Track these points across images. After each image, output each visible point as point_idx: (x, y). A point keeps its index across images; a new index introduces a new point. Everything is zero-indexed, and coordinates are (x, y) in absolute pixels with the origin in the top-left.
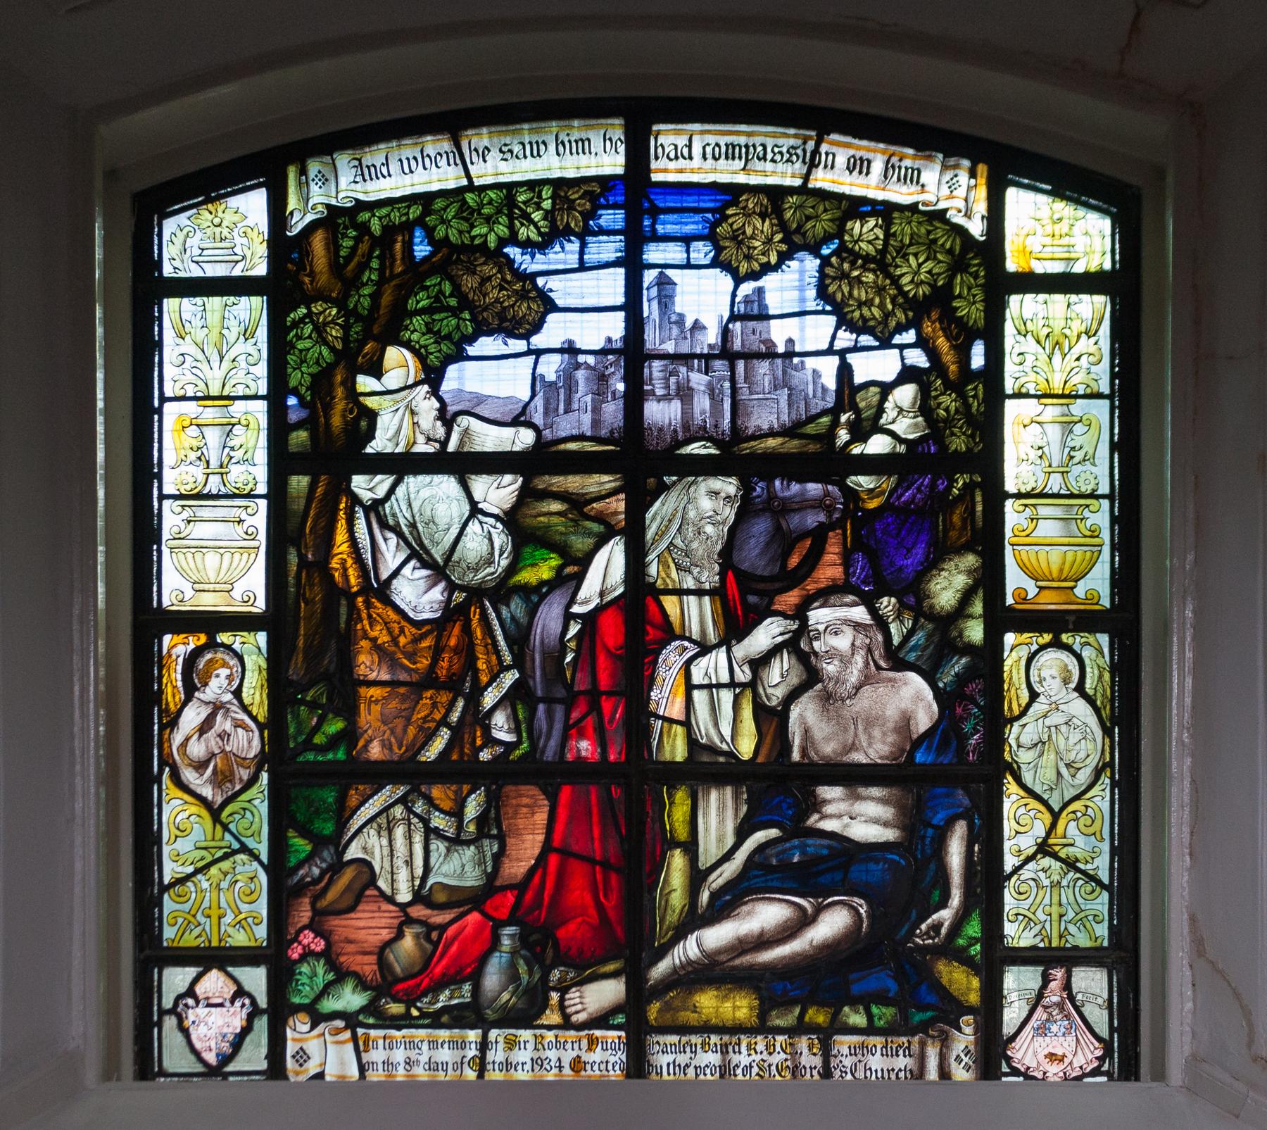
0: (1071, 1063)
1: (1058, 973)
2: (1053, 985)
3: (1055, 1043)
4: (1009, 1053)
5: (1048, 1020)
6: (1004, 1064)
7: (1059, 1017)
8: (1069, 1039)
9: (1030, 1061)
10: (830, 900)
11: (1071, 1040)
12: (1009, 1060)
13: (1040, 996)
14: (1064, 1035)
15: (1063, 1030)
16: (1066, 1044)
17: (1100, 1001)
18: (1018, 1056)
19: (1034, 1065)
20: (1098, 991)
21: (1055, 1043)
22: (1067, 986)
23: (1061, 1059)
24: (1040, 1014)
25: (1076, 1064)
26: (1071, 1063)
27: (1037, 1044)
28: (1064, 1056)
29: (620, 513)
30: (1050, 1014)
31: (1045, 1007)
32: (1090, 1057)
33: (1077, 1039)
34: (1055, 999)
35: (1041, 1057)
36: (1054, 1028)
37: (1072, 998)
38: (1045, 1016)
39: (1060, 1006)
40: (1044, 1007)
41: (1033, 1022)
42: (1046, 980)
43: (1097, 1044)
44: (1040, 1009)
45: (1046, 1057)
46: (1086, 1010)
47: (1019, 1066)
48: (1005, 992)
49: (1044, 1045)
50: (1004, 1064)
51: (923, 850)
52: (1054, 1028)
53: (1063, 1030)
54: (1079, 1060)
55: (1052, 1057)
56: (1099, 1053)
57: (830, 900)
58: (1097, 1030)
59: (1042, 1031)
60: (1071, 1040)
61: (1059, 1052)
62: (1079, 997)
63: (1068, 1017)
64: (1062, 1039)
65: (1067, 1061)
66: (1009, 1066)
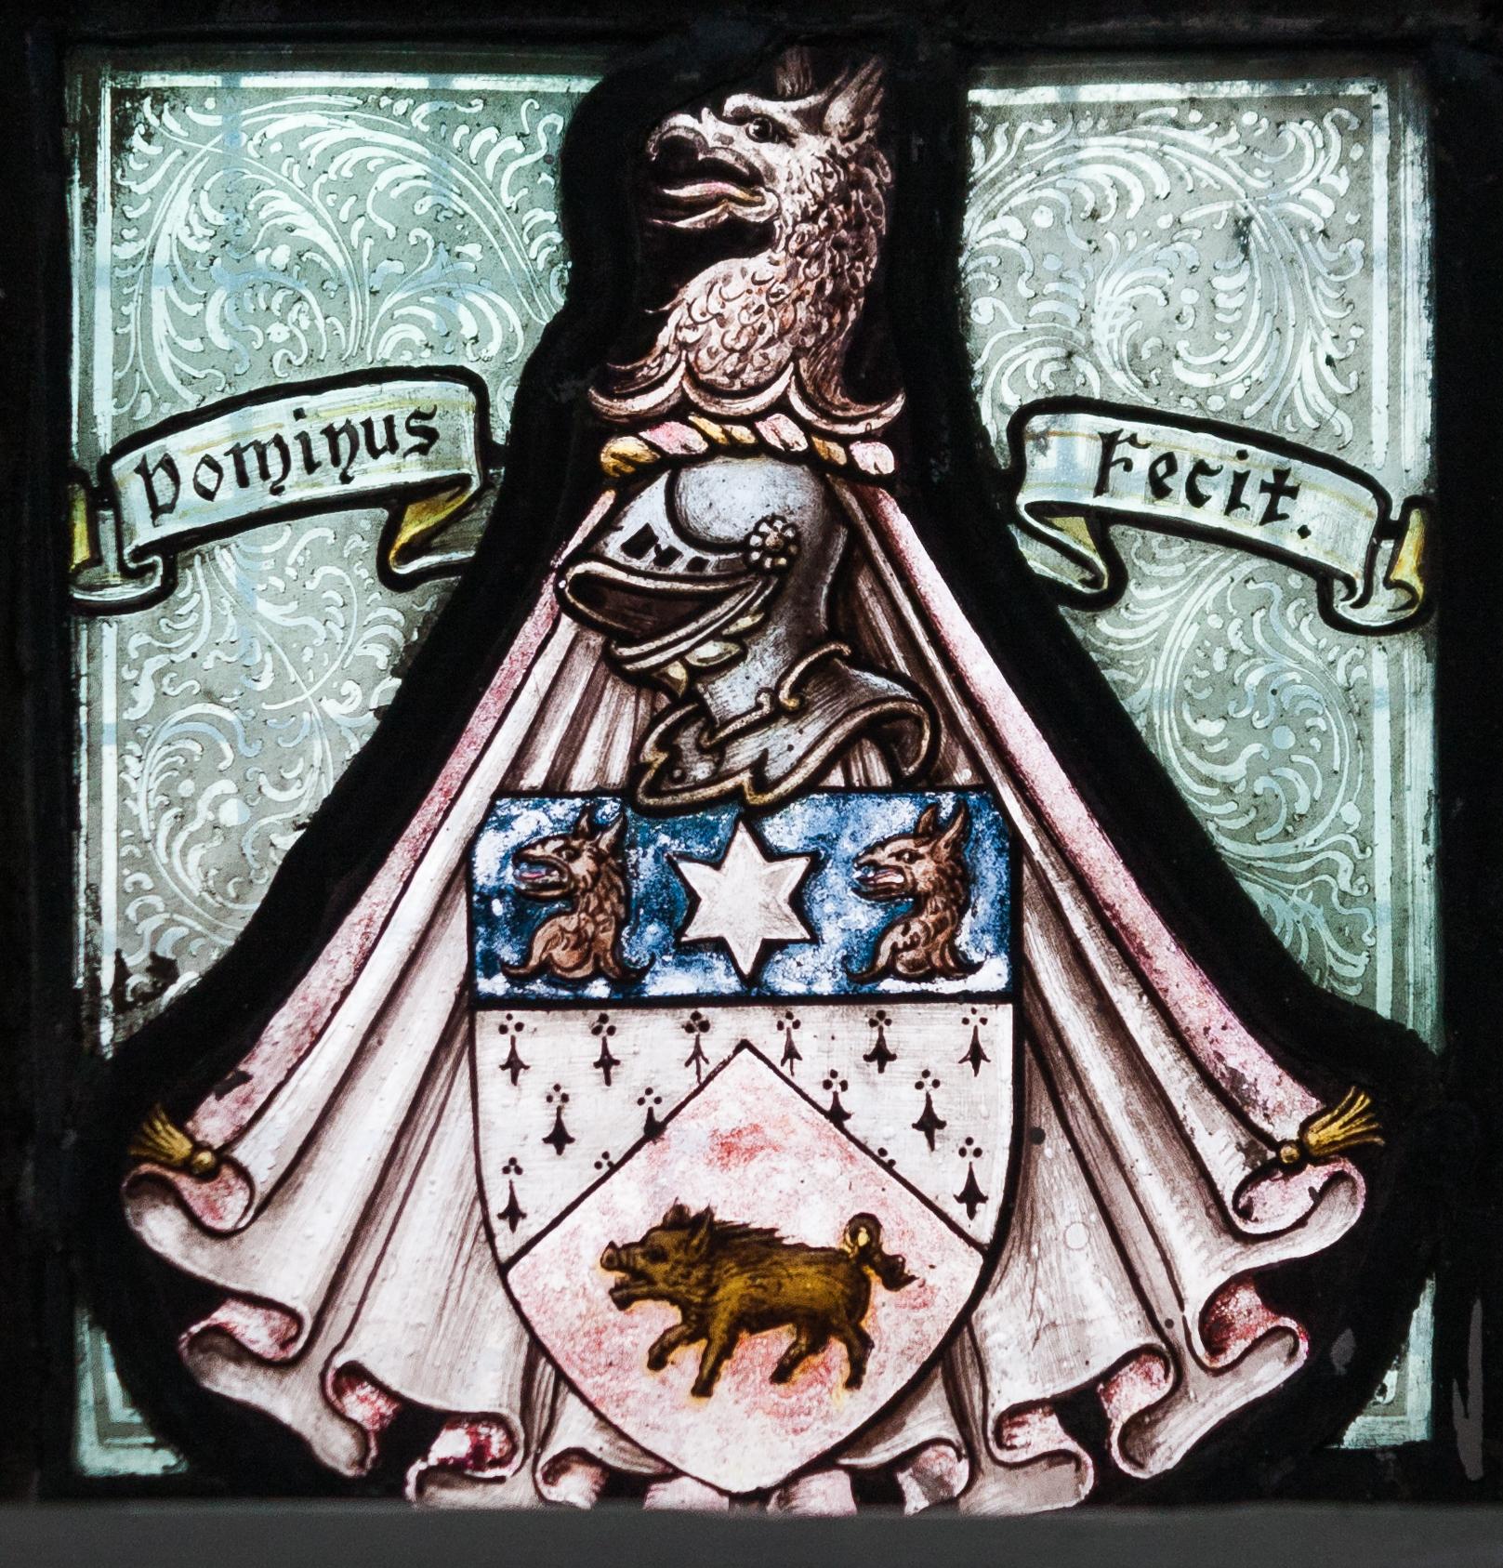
0: (953, 1360)
1: (786, 155)
2: (721, 310)
3: (743, 1093)
4: (161, 1230)
5: (649, 792)
6: (102, 1382)
7: (792, 747)
8: (927, 1034)
9: (428, 1335)
10: (373, 1444)
11: (950, 1054)
12: (164, 1319)
13: (553, 448)
14: (860, 986)
15: (846, 916)
16: (884, 1108)
17: (1329, 521)
18: (288, 1261)
19: (487, 1383)
20: (1308, 405)
21: (743, 1093)
22: (901, 324)
23: (824, 1302)
24: (549, 702)
25: (1015, 1375)
26: (953, 1360)
27: (515, 1116)
28: (867, 1262)
29: (1166, 475)
30: (682, 708)
31: (618, 617)
32: (1202, 1265)
33: (1039, 1052)
34: (739, 498)
35: (566, 1281)
36: (738, 895)
37: (963, 487)
38: (608, 750)
39: (812, 589)
40: (600, 606)
41: (463, 825)
42: (626, 234)
43: (1285, 1105)
44: (545, 652)
45: (633, 1271)
46: (1162, 632)
47: (291, 1403)
48: (101, 410)
49: (605, 1118)
50: (102, 1382)
51: (1228, 817)
52: (738, 895)
53: (846, 916)
54: (1063, 1319)
55: (706, 1278)
56: (1310, 1219)
57: (373, 1444)
58: (1288, 913)
59: (581, 936)
60: (950, 1054)
61: (804, 1203)
62: (1060, 465)
63: (910, 739)
64: (832, 1038)
65: (901, 1329)
66: (171, 1401)
